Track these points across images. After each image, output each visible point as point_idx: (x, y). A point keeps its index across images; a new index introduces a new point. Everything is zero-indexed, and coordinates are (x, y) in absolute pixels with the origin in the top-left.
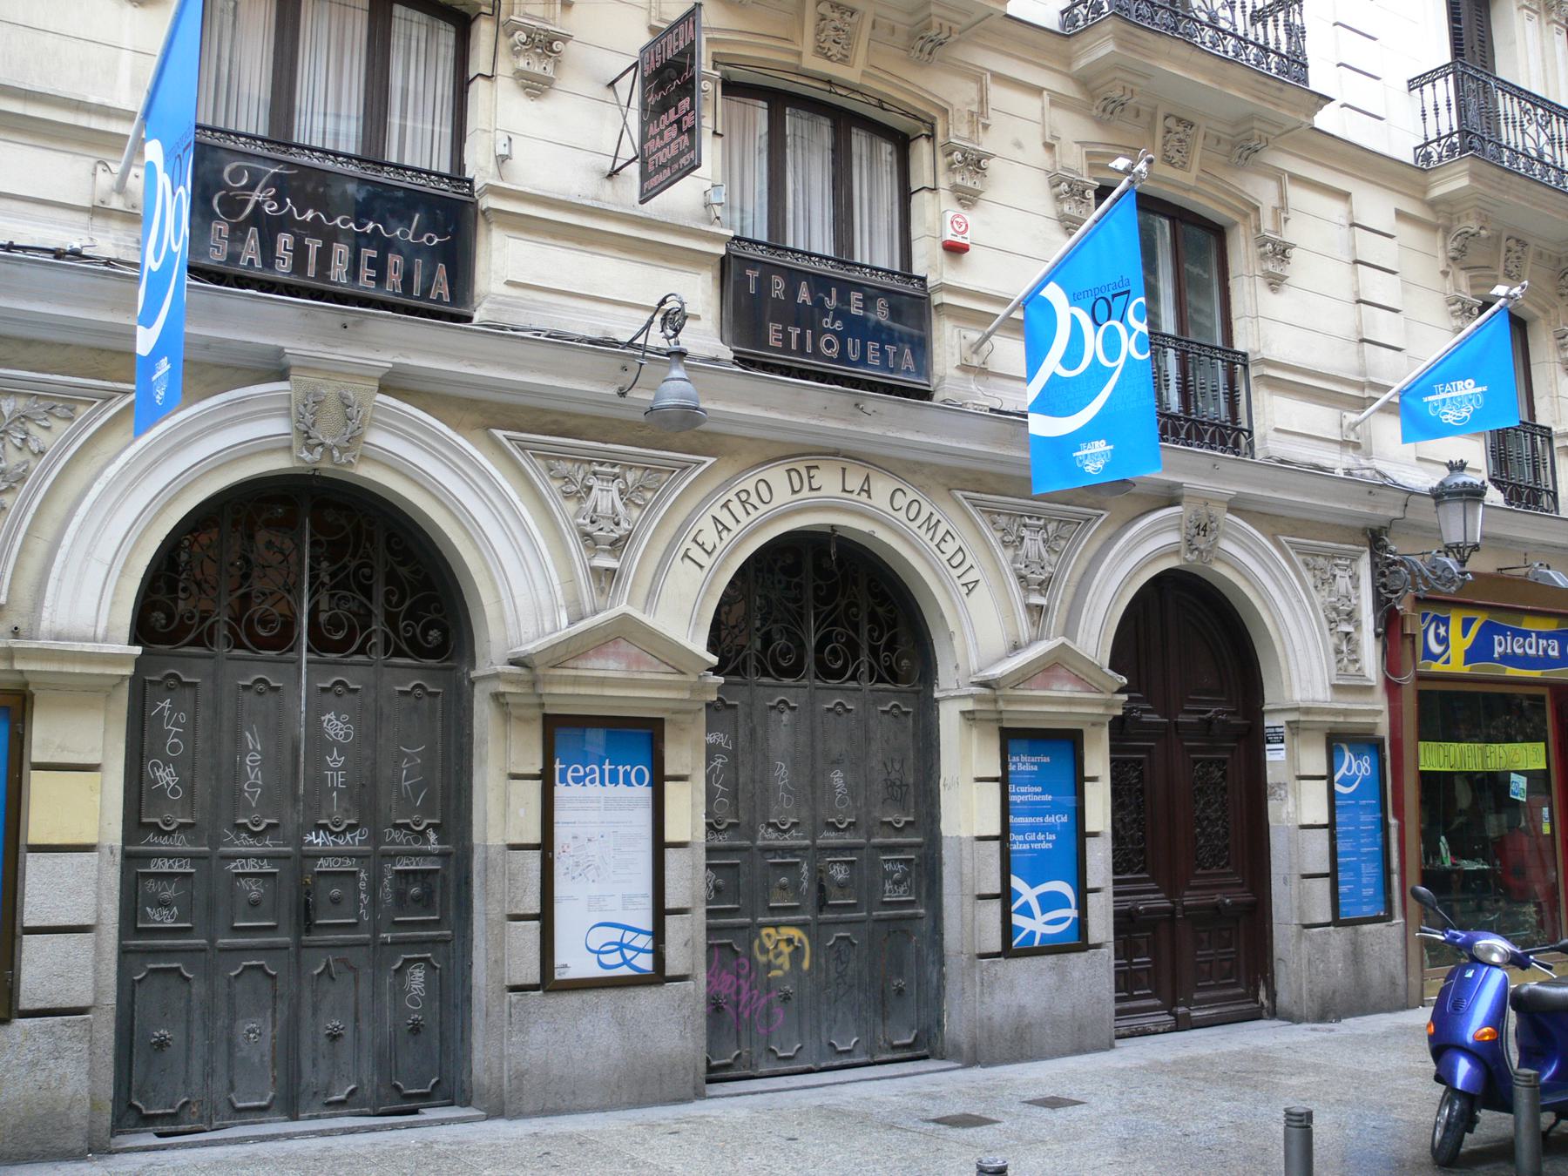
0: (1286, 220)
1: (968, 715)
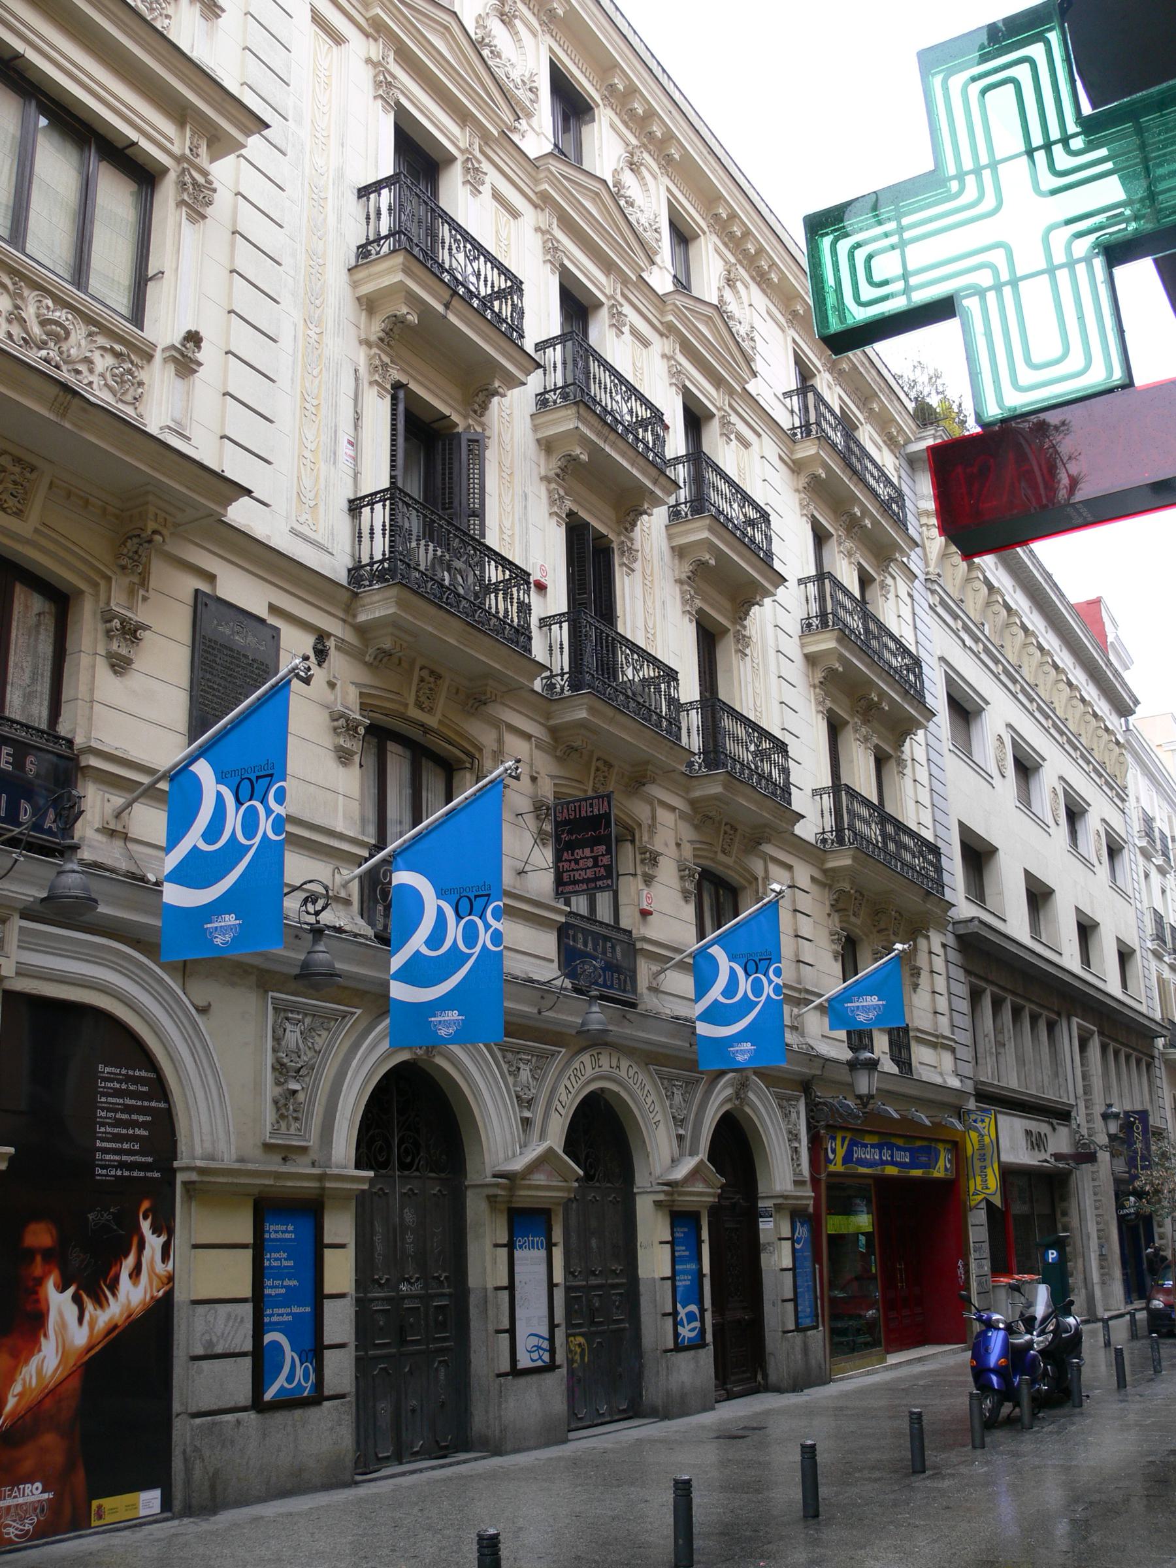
0: (145, 599)
1: (658, 1204)
